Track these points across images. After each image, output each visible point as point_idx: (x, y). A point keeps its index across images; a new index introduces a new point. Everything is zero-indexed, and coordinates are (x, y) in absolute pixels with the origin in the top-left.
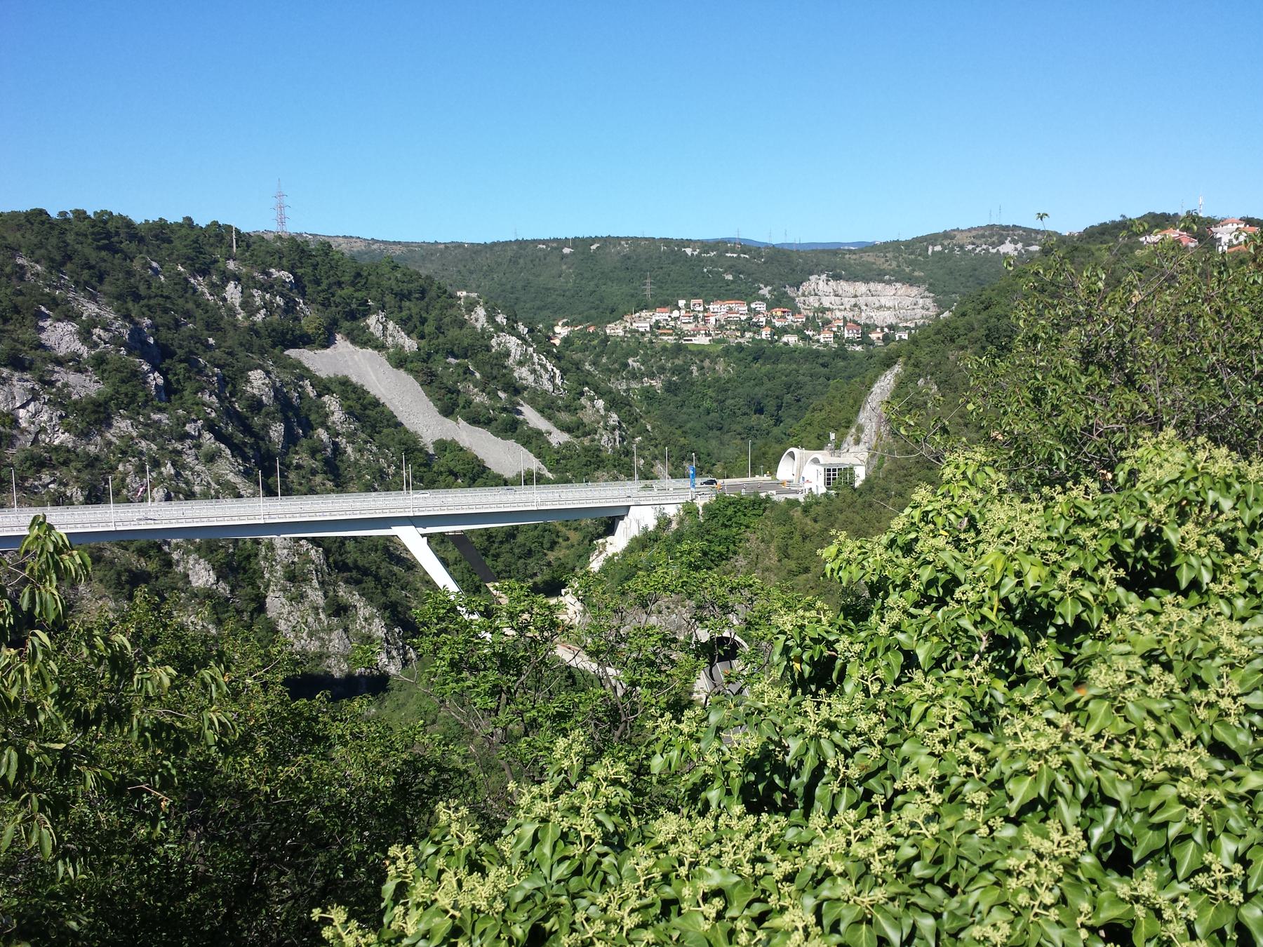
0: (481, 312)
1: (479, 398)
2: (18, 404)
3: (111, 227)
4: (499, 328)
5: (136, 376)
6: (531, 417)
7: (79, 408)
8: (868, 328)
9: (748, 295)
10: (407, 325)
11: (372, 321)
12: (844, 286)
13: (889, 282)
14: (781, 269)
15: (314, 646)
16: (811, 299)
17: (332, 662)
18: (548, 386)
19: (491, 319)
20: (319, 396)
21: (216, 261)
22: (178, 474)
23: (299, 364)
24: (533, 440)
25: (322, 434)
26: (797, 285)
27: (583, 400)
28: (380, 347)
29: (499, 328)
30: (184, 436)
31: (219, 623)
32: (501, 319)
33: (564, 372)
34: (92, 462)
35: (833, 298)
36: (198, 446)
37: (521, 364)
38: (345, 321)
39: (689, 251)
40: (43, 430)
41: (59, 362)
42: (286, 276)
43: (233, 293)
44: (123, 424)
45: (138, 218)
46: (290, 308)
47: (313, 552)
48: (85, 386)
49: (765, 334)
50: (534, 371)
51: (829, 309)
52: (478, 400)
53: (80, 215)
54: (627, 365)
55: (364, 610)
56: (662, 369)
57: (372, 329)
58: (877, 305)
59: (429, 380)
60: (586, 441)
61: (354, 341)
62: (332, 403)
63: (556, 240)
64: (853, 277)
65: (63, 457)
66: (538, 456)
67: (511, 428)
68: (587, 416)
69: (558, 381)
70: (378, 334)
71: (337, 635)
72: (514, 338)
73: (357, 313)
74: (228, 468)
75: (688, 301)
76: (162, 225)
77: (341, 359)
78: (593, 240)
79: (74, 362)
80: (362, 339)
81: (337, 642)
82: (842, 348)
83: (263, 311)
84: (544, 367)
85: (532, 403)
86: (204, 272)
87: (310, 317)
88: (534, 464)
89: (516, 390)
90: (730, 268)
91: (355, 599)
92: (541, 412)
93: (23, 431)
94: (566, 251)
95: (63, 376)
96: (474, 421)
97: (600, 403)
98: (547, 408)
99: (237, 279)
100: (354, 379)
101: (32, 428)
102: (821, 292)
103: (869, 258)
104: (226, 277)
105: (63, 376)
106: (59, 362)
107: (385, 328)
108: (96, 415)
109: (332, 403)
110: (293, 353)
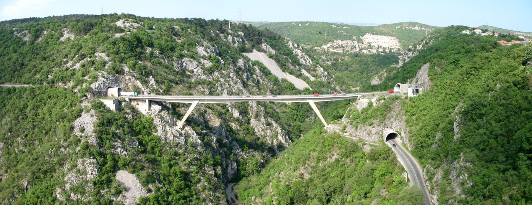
0: (290, 43)
1: (292, 67)
3: (201, 22)
5: (218, 61)
6: (304, 71)
8: (385, 48)
9: (350, 38)
10: (273, 46)
11: (263, 45)
12: (375, 37)
13: (387, 36)
14: (359, 31)
15: (263, 134)
17: (267, 138)
18: (308, 64)
19: (293, 45)
20: (253, 65)
21: (226, 30)
22: (229, 87)
23: (247, 58)
24: (306, 79)
25: (255, 76)
26: (363, 36)
27: (317, 68)
28: (265, 52)
30: (230, 77)
31: (240, 126)
32: (296, 45)
33: (312, 60)
34: (210, 83)
36: (233, 80)
37: (301, 58)
38: (256, 45)
39: (333, 26)
40: (199, 75)
41: (200, 57)
42: (242, 34)
43: (230, 38)
44: (217, 74)
45: (207, 19)
46: (243, 42)
48: (208, 64)
49: (358, 50)
50: (305, 60)
52: (291, 68)
53: (217, 20)
54: (321, 58)
55: (275, 125)
56: (331, 60)
59: (278, 61)
60: (319, 80)
61: (259, 51)
62: (257, 68)
64: (377, 34)
65: (203, 82)
66: (308, 83)
67: (300, 76)
69: (311, 63)
70: (265, 49)
71: (269, 131)
73: (259, 43)
76: (212, 20)
77: (255, 56)
78: (307, 22)
79: (204, 57)
81: (269, 132)
82: (379, 54)
86: (223, 33)
87: (248, 45)
88: (307, 86)
89: (299, 65)
90: (345, 31)
91: (273, 122)
92: (307, 71)
93: (195, 75)
94: (300, 25)
95: (203, 61)
96: (291, 73)
98: (308, 71)
99: (231, 34)
100: (260, 61)
101: (197, 74)
102: (368, 38)
103: (381, 29)
104: (228, 34)
105: (203, 61)
106: (200, 57)
108: (210, 71)
109: (257, 68)
110: (244, 54)
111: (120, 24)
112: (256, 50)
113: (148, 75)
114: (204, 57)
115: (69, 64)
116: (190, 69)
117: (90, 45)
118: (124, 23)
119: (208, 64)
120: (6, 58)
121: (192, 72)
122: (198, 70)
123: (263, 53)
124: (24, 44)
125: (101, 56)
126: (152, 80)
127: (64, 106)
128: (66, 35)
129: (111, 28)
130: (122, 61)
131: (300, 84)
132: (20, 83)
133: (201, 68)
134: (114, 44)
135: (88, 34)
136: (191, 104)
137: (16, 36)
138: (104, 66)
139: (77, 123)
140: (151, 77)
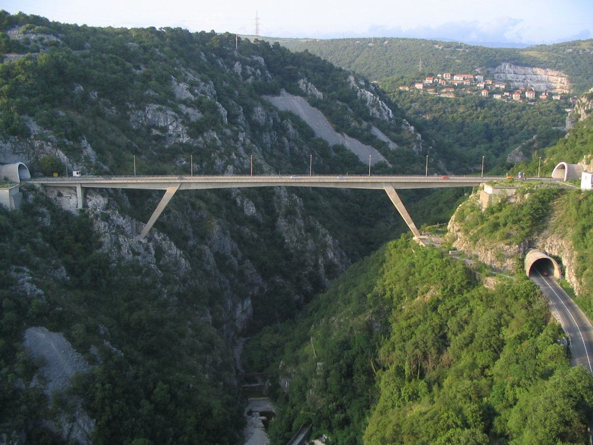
1: (354, 124)
2: (169, 123)
4: (361, 87)
6: (376, 131)
7: (191, 125)
10: (319, 85)
11: (301, 82)
12: (519, 69)
16: (502, 75)
18: (386, 118)
24: (380, 147)
29: (361, 87)
35: (512, 75)
37: (372, 106)
47: (298, 200)
48: (195, 115)
49: (484, 93)
50: (379, 110)
51: (511, 81)
52: (353, 124)
57: (300, 87)
58: (537, 79)
59: (328, 113)
63: (364, 39)
65: (187, 149)
67: (369, 140)
68: (406, 135)
71: (310, 242)
72: (369, 93)
74: (257, 156)
75: (442, 74)
77: (285, 102)
80: (295, 91)
83: (252, 77)
84: (384, 108)
85: (378, 127)
88: (382, 159)
95: (183, 107)
96: (352, 135)
97: (412, 128)
98: (385, 130)
103: (533, 54)
107: (307, 86)
112: (287, 91)
113: (75, 136)
116: (162, 124)
119: (195, 115)
121: (164, 129)
122: (177, 127)
123: (299, 98)
131: (369, 155)
133: (183, 123)
136: (164, 192)
140: (85, 142)
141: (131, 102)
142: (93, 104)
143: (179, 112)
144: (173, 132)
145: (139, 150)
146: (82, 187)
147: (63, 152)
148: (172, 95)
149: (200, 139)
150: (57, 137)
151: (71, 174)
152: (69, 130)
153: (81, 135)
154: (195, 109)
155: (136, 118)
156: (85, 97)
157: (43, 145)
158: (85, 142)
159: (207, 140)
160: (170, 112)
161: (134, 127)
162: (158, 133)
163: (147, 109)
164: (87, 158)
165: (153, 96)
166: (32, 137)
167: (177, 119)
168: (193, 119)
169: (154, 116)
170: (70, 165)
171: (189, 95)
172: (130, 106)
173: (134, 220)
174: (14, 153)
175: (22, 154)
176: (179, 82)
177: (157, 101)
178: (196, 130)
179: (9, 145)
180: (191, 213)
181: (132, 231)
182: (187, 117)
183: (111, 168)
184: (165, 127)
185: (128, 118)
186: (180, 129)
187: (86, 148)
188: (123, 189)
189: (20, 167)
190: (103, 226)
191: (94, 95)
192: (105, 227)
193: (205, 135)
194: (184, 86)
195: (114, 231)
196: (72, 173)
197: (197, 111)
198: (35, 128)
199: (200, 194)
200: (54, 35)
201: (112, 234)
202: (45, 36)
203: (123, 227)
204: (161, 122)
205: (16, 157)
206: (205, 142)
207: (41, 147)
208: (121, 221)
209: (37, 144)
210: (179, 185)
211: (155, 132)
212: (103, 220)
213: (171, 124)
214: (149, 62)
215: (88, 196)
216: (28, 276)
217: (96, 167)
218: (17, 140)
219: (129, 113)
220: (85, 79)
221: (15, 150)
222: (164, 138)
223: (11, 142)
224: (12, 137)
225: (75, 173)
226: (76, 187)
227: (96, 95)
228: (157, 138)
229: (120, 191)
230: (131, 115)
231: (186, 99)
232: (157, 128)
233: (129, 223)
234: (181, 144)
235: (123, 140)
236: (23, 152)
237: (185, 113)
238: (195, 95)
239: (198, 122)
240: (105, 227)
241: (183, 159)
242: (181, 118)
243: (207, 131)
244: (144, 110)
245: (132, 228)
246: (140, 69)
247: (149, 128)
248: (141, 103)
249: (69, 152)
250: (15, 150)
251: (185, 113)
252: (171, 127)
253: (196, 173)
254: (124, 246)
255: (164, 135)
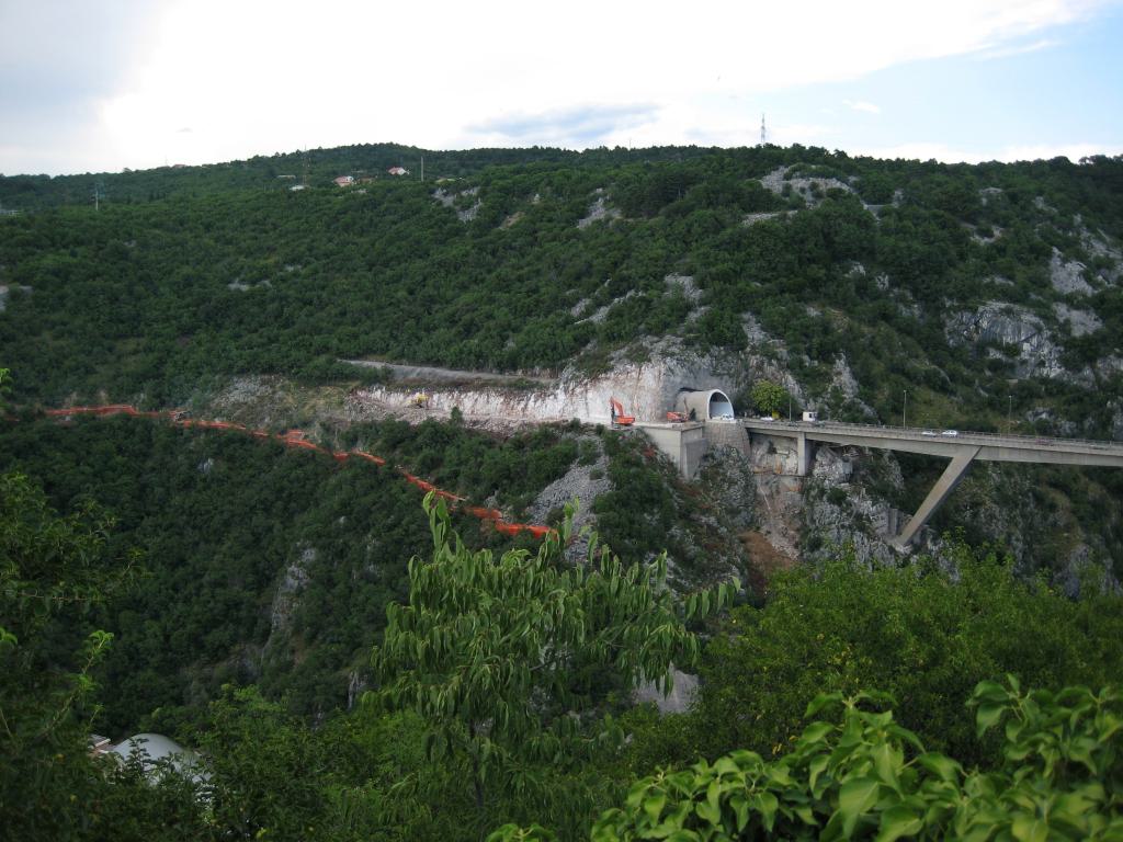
7: (1070, 344)
48: (1084, 324)
65: (1055, 388)
79: (1071, 301)
95: (1062, 310)
111: (773, 182)
113: (826, 354)
114: (1071, 301)
115: (576, 311)
116: (1008, 340)
117: (656, 249)
118: (787, 177)
119: (1084, 324)
120: (389, 273)
121: (1013, 350)
122: (1040, 346)
124: (459, 232)
125: (683, 284)
126: (844, 377)
127: (145, 207)
128: (599, 212)
129: (737, 197)
130: (744, 302)
132: (414, 361)
133: (1053, 339)
134: (736, 244)
135: (663, 210)
136: (946, 462)
137: (440, 203)
138: (682, 319)
139: (550, 494)
140: (840, 364)
141: (951, 297)
142: (877, 296)
143: (1049, 318)
144: (1031, 355)
145: (952, 386)
146: (806, 440)
147: (794, 378)
148: (1042, 284)
149: (1087, 372)
150: (789, 352)
151: (800, 416)
152: (816, 341)
153: (836, 352)
154: (1088, 314)
155: (958, 326)
156: (863, 287)
157: (763, 363)
158: (840, 364)
159: (1102, 374)
160: (1029, 318)
161: (951, 341)
162: (998, 356)
163: (981, 309)
164: (837, 392)
165: (1001, 285)
166: (748, 349)
167: (1039, 330)
168: (1077, 332)
169: (993, 323)
170: (803, 401)
171: (1083, 286)
172: (948, 304)
173: (895, 511)
174: (714, 374)
175: (726, 377)
176: (1065, 260)
177: (1004, 295)
178: (1081, 352)
179: (707, 359)
180: (1031, 513)
181: (889, 528)
182: (1066, 327)
183: (879, 411)
184: (1014, 345)
185: (941, 326)
186: (1046, 351)
187: (839, 373)
188: (893, 451)
189: (716, 398)
190: (829, 510)
191: (883, 281)
192: (832, 513)
193: (1099, 365)
194: (1075, 267)
195: (847, 523)
196: (802, 414)
197: (1094, 316)
198: (755, 334)
199: (1062, 479)
200: (838, 180)
201: (843, 527)
202: (820, 181)
203: (868, 519)
204: (1007, 335)
205: (715, 381)
206: (1098, 379)
207: (760, 367)
208: (866, 506)
209: (753, 361)
210: (975, 451)
211: (994, 354)
212: (831, 500)
213: (1027, 340)
214: (1012, 222)
215: (818, 457)
216: (670, 573)
217: (848, 408)
218: (723, 353)
219: (943, 316)
220: (868, 254)
221: (716, 368)
222: (1012, 367)
223: (711, 356)
224: (715, 347)
225: (806, 416)
226: (796, 439)
227: (887, 283)
228: (996, 366)
229: (887, 455)
230: (947, 321)
231: (1072, 293)
232: (999, 347)
233: (884, 514)
234: (1045, 381)
235: (923, 365)
236: (728, 374)
237: (1061, 320)
238: (1095, 285)
239: (1086, 337)
240: (832, 513)
241: (1040, 409)
242: (1050, 329)
243: (1105, 356)
244: (974, 311)
245: (889, 522)
246: (990, 235)
247: (981, 348)
248: (969, 298)
249: (805, 377)
250: (716, 368)
251: (1061, 320)
252: (1026, 346)
253: (1072, 436)
254: (860, 552)
255: (1010, 361)
